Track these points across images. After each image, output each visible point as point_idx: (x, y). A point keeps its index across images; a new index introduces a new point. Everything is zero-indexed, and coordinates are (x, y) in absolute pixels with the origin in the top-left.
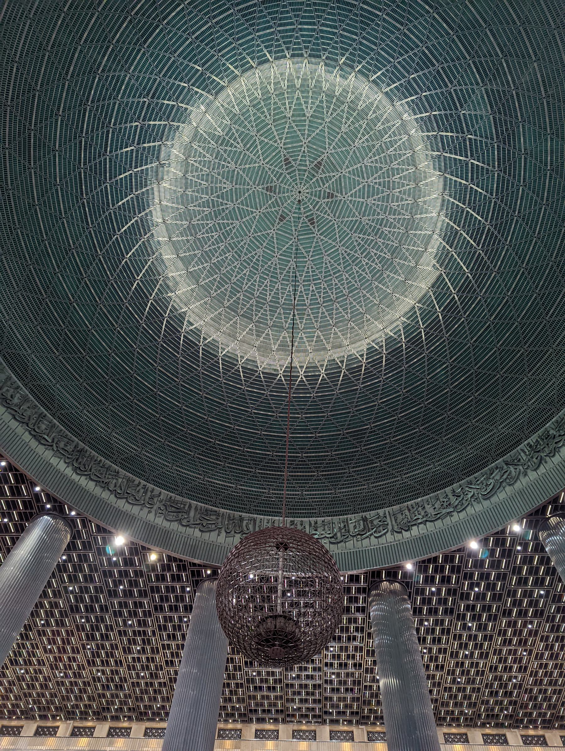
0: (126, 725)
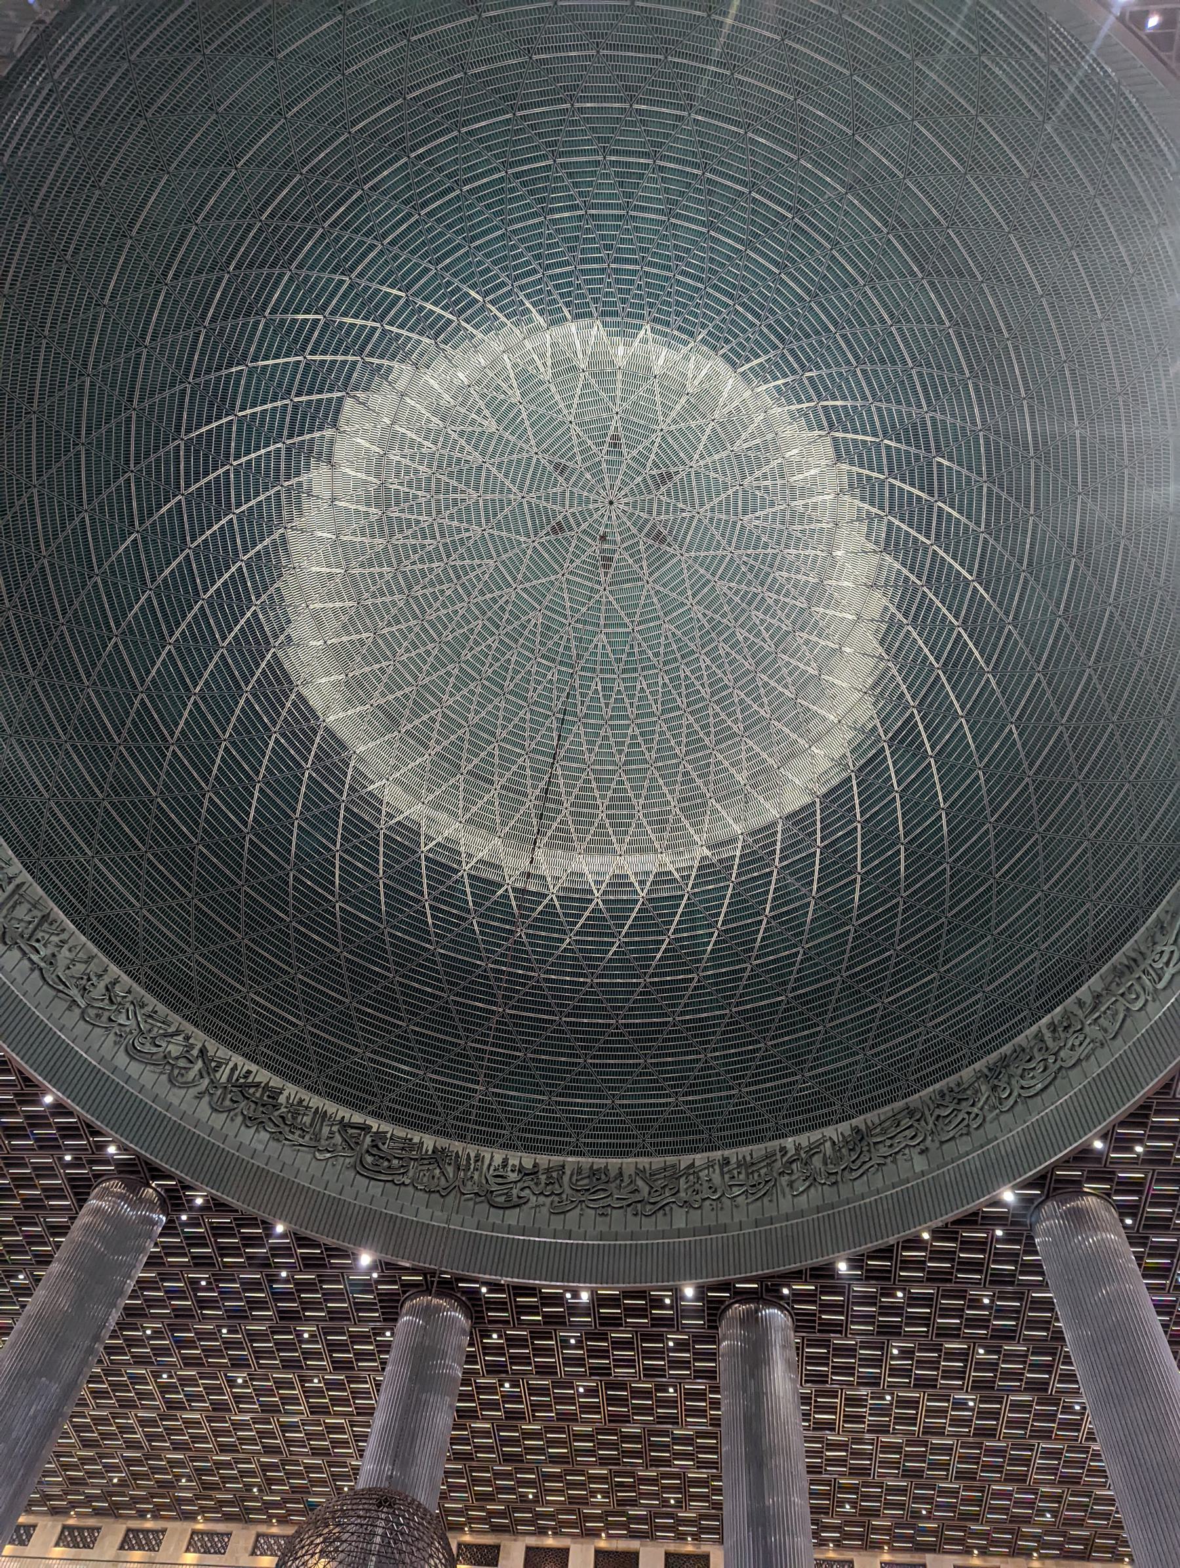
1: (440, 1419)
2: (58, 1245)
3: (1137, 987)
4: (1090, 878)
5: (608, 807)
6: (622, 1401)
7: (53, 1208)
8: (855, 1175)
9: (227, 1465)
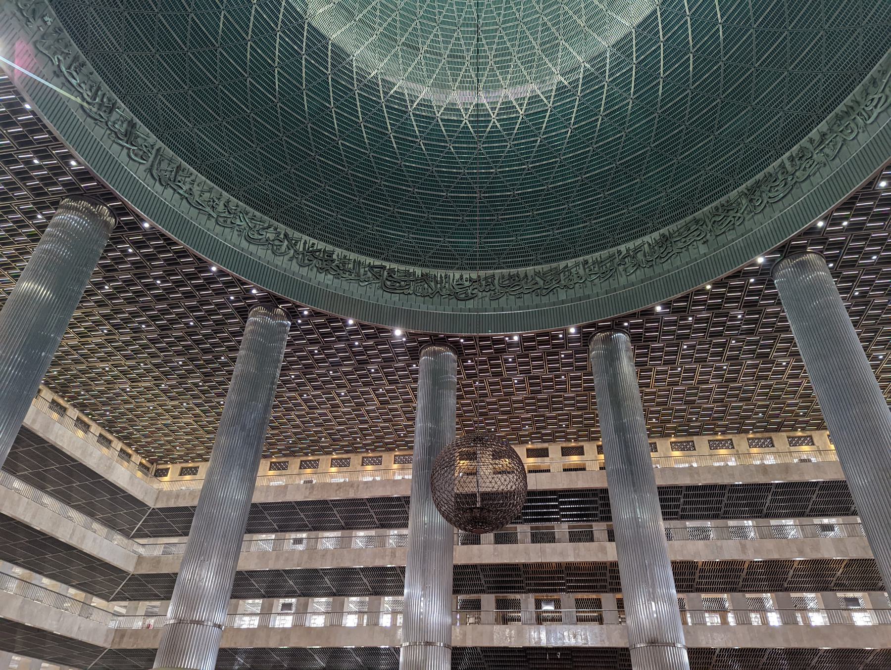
1: (451, 401)
2: (239, 342)
3: (852, 125)
4: (823, 57)
5: (495, 56)
6: (538, 384)
7: (231, 323)
8: (663, 260)
9: (343, 430)
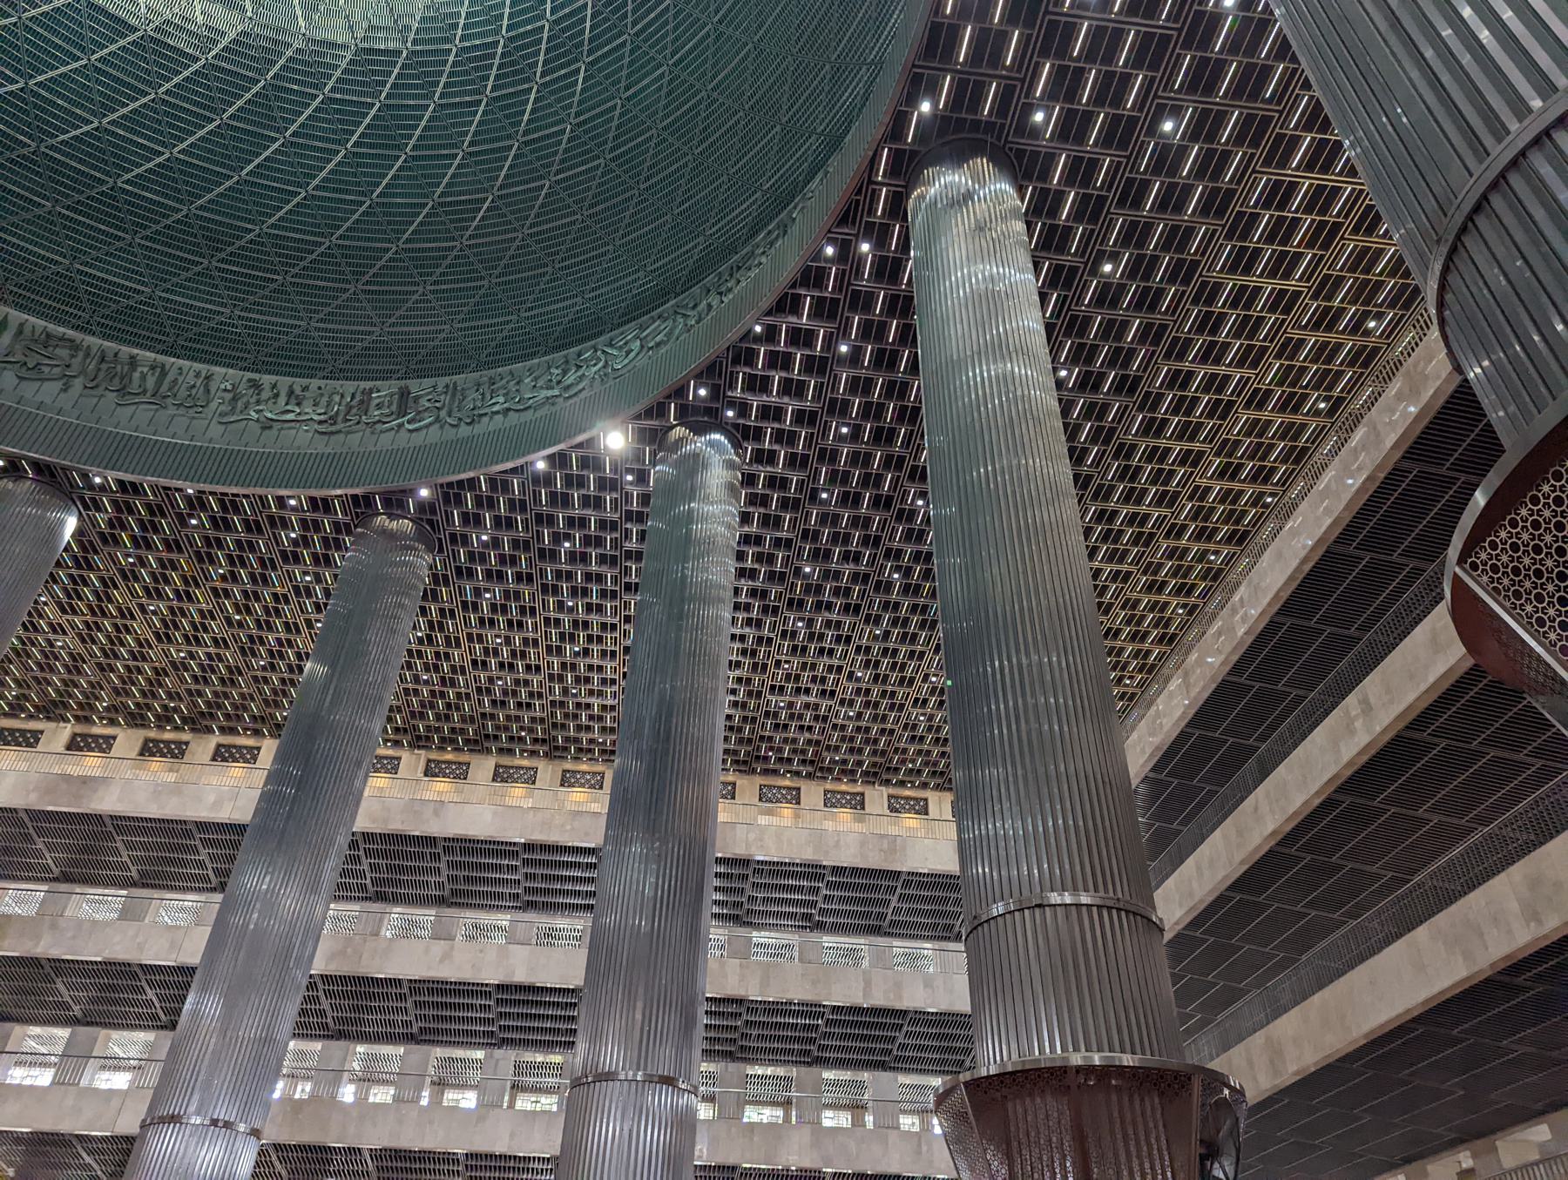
0: (250, 742)
4: (626, 221)
